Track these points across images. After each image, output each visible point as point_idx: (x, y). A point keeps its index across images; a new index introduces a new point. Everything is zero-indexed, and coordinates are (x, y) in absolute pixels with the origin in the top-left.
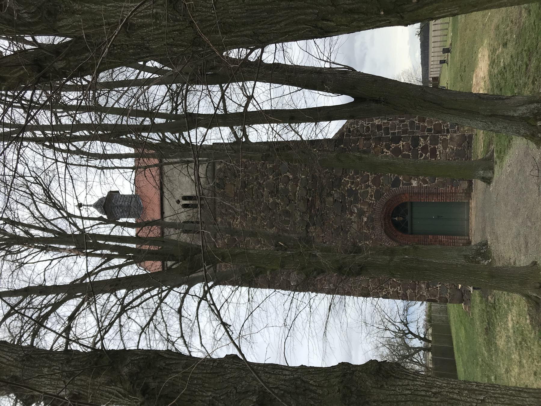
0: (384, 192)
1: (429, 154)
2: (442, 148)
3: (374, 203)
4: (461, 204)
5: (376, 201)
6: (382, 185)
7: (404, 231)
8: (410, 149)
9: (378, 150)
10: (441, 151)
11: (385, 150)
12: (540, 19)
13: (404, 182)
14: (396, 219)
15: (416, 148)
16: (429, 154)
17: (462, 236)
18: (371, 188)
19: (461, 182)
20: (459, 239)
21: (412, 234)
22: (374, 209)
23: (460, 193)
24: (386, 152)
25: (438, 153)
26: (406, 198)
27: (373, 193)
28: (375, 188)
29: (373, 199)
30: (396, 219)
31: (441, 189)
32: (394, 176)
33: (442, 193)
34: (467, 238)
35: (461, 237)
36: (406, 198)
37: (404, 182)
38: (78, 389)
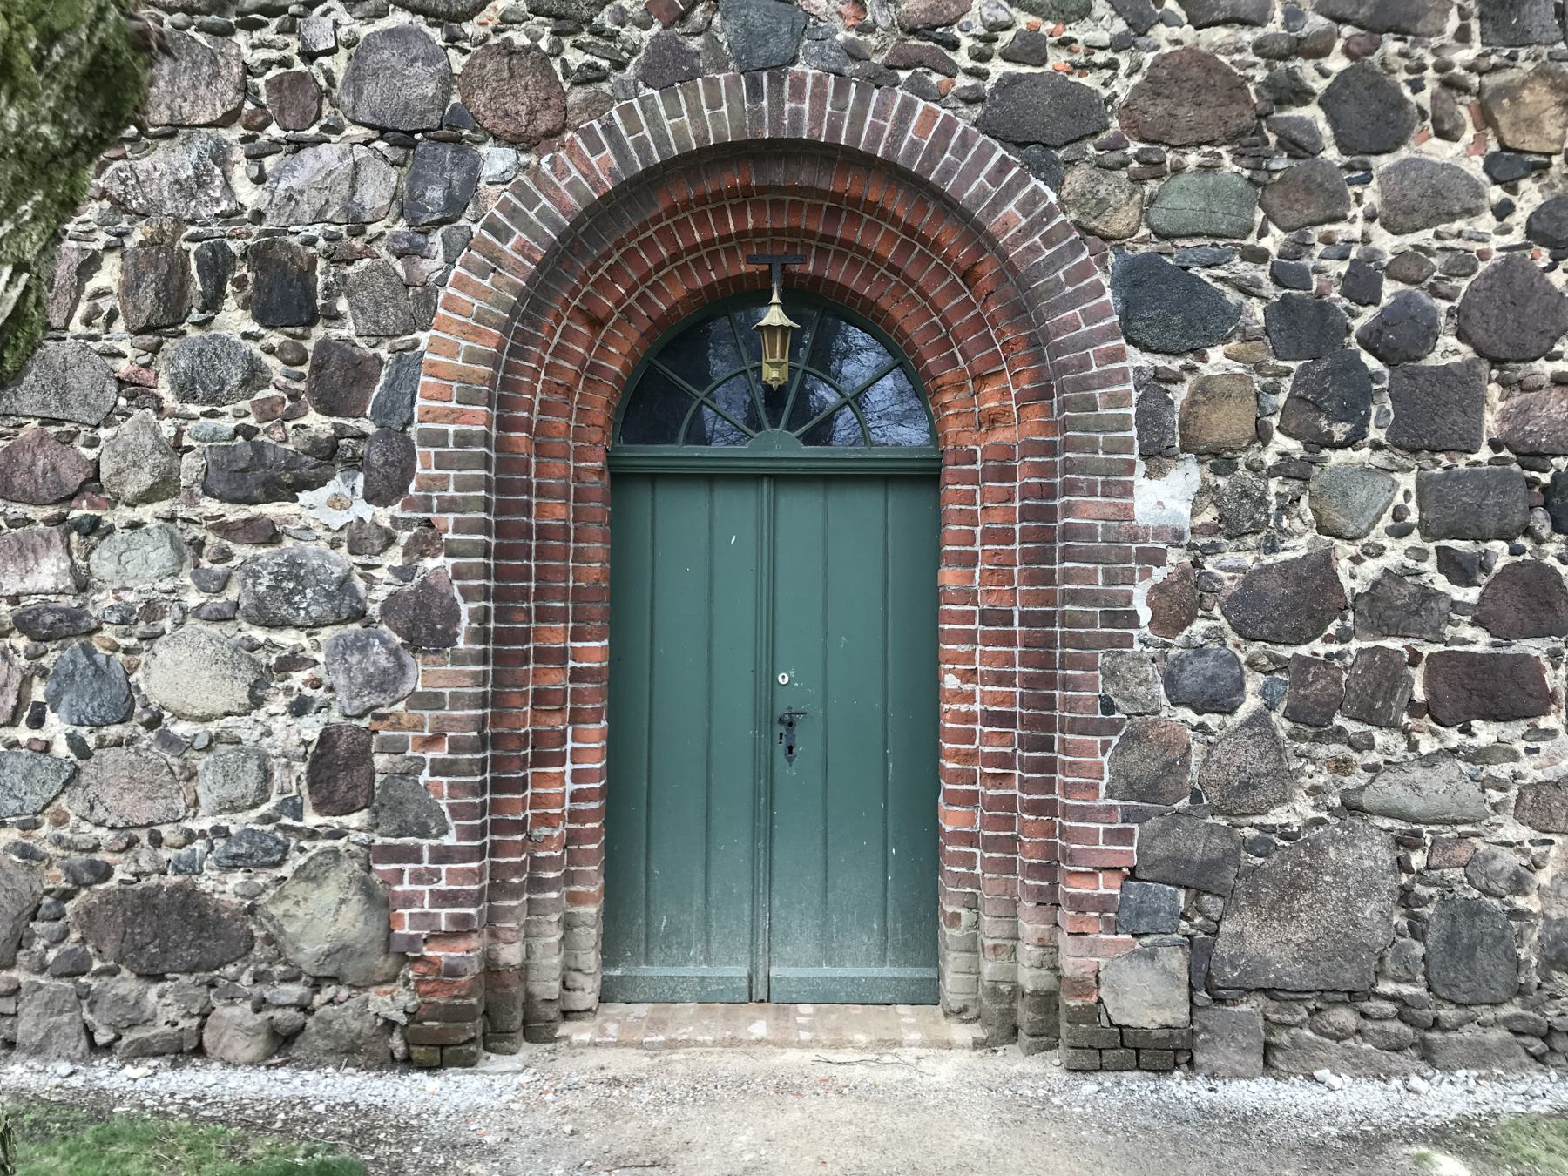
0: (1076, 179)
1: (1481, 642)
2: (1531, 770)
3: (950, 71)
4: (919, 931)
5: (972, 98)
6: (1153, 168)
7: (655, 401)
8: (1533, 457)
9: (1533, 123)
10: (1503, 770)
11: (1530, 196)
12: (2, 472)
13: (1180, 394)
14: (774, 316)
15: (1541, 521)
16: (1481, 642)
17: (611, 950)
18: (1118, 44)
19: (1177, 961)
20: (568, 924)
21: (621, 477)
22: (882, 78)
23: (1049, 946)
24: (1503, 211)
25: (1485, 733)
26: (992, 420)
27: (1057, 60)
28: (1123, 88)
29: (998, 68)
30: (774, 316)
31: (1094, 764)
32: (1248, 289)
33: (1048, 766)
34: (586, 996)
35: (589, 937)
36: (992, 420)
37: (1180, 394)
38: (504, 206)
